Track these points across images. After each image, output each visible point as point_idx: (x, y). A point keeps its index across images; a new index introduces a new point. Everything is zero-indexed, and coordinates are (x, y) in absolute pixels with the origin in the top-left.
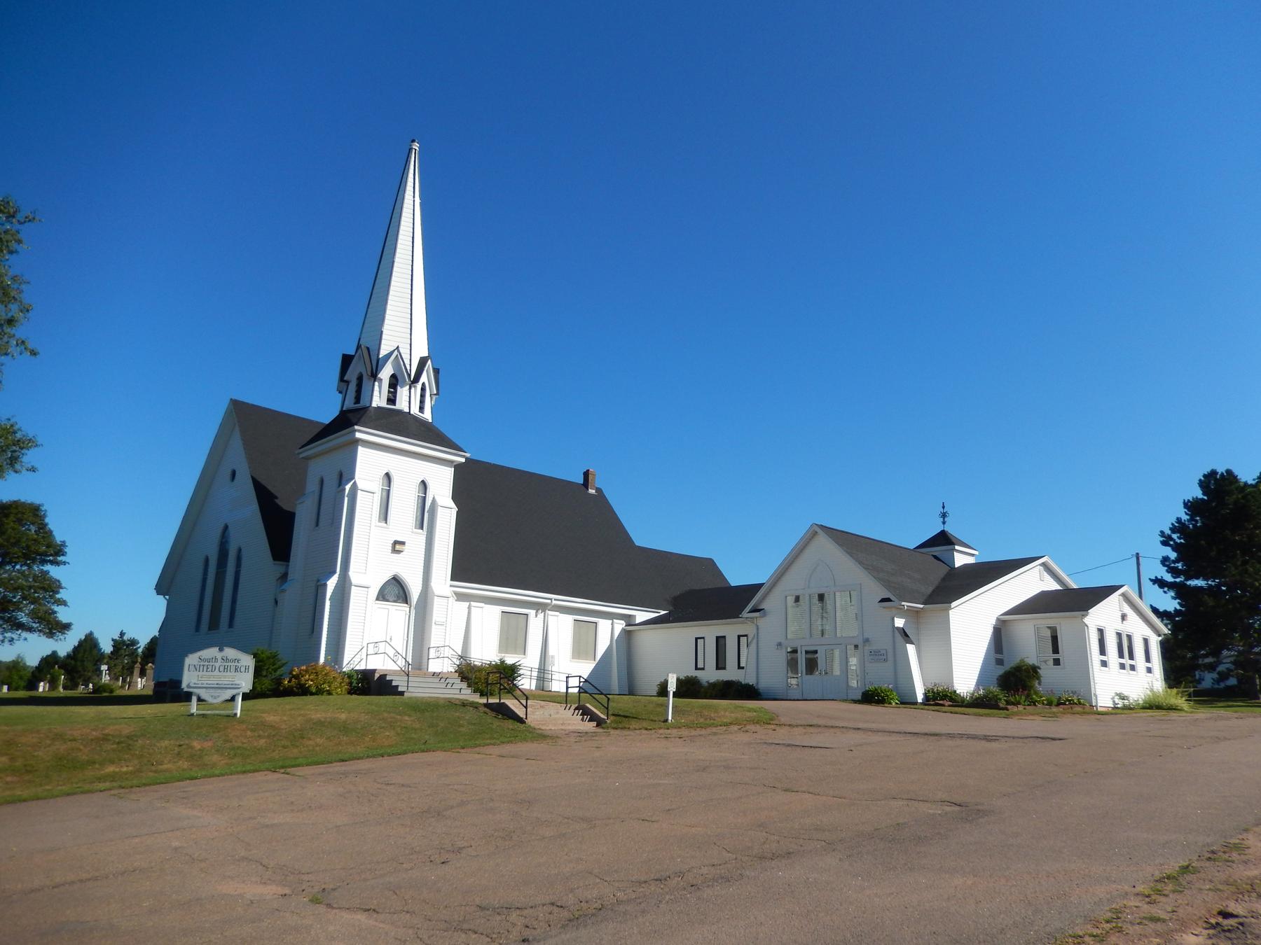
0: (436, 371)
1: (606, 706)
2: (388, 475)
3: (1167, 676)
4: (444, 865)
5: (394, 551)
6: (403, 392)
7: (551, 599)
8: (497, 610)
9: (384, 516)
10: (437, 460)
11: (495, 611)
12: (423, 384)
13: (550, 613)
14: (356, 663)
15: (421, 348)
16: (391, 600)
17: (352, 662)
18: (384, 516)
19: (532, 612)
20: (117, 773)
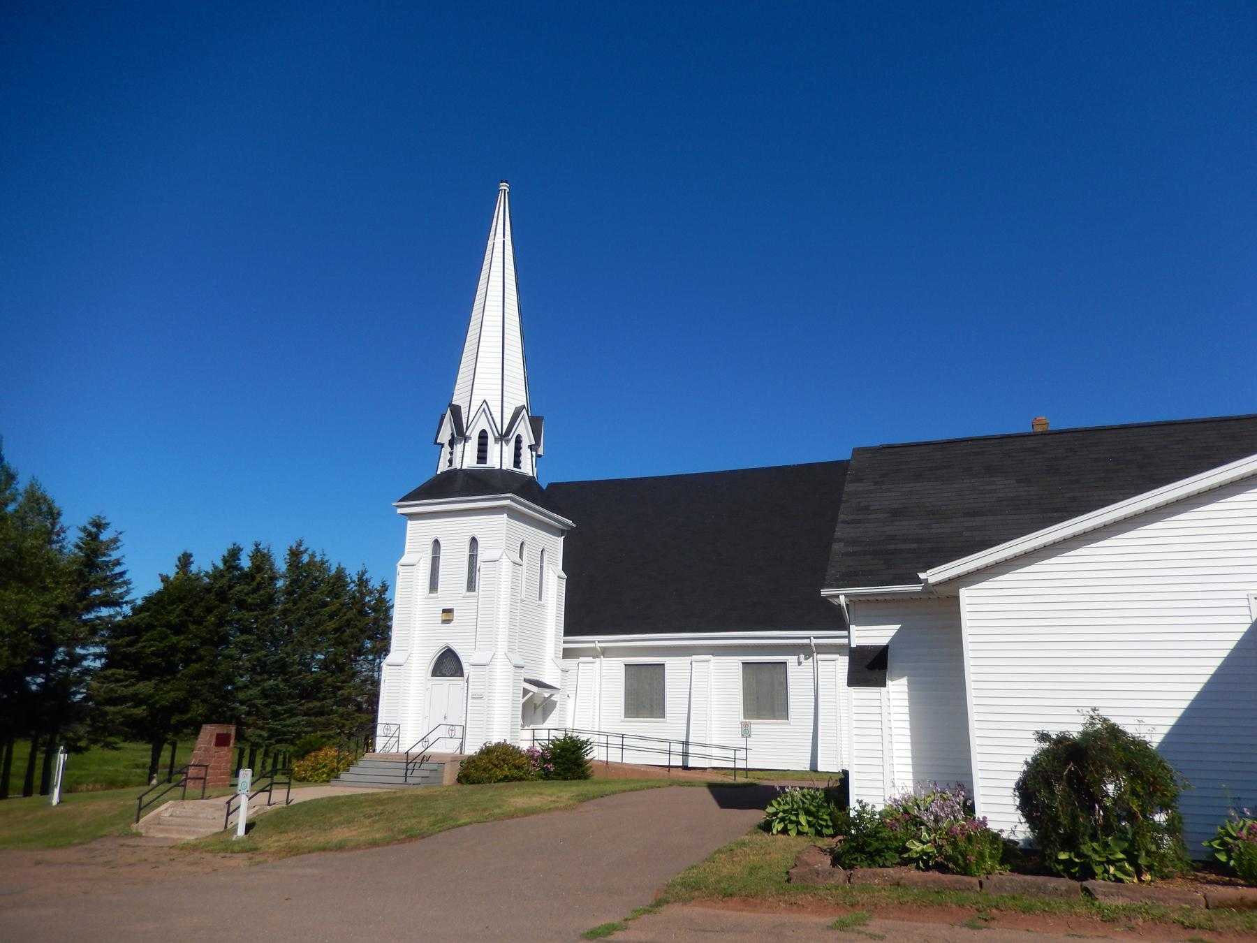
0: (532, 420)
1: (142, 806)
2: (436, 542)
3: (375, 699)
4: (1027, 932)
5: (445, 621)
6: (493, 449)
7: (809, 638)
8: (735, 663)
9: (433, 586)
10: (448, 514)
11: (734, 664)
12: (519, 436)
13: (820, 656)
14: (391, 746)
15: (517, 396)
16: (447, 674)
17: (388, 745)
18: (433, 586)
19: (791, 660)
20: (1095, 812)
